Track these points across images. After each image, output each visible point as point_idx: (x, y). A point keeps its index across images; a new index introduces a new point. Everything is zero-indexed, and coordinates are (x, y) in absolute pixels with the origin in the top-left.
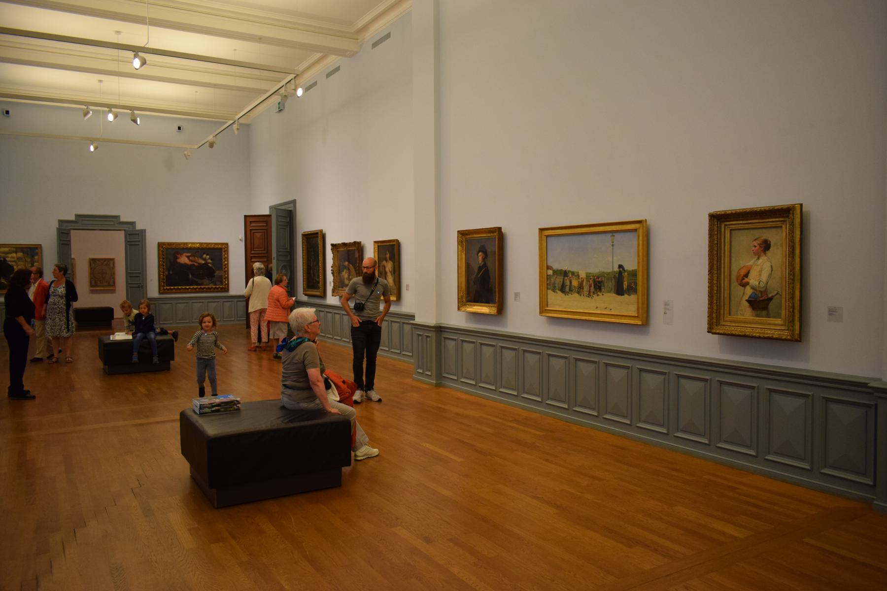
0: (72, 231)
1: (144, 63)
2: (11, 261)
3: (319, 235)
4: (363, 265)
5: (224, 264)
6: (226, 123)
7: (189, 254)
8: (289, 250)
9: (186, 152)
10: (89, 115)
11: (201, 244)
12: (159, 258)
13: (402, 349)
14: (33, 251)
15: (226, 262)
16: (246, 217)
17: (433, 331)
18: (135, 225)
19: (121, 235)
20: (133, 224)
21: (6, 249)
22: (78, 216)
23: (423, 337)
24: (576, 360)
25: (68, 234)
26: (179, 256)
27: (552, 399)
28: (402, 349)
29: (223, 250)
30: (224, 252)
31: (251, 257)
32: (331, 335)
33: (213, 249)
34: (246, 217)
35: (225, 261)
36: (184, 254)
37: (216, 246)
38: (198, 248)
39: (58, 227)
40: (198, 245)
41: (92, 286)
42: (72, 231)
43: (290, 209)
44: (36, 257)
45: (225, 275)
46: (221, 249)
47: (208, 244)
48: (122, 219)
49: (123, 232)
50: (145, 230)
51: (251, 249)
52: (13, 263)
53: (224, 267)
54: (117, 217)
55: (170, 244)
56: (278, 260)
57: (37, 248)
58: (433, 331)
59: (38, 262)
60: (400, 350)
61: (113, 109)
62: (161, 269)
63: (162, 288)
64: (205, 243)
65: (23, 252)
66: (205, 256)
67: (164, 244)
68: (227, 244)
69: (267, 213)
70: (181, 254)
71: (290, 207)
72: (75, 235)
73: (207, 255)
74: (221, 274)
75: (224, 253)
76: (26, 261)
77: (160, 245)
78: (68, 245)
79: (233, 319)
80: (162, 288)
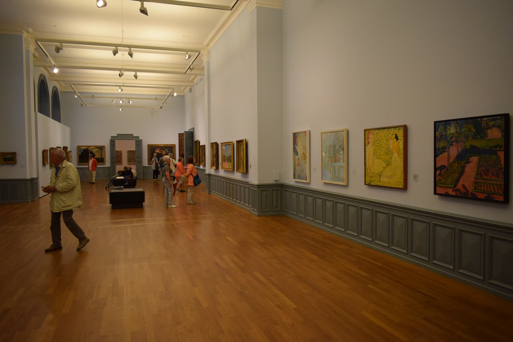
0: (116, 140)
1: (122, 90)
2: (94, 152)
4: (503, 152)
7: (159, 149)
8: (192, 147)
9: (155, 109)
10: (114, 102)
11: (165, 145)
12: (148, 152)
14: (101, 148)
16: (179, 134)
17: (256, 187)
19: (134, 141)
20: (138, 137)
21: (92, 148)
22: (118, 135)
23: (333, 203)
24: (393, 216)
25: (114, 141)
26: (156, 150)
27: (415, 252)
30: (174, 148)
31: (181, 150)
33: (169, 147)
34: (179, 134)
36: (158, 149)
37: (171, 146)
38: (163, 147)
39: (110, 139)
40: (163, 145)
41: (128, 162)
42: (116, 140)
44: (103, 151)
46: (172, 147)
47: (167, 145)
48: (134, 135)
49: (135, 140)
50: (142, 140)
52: (95, 153)
54: (132, 135)
55: (152, 145)
57: (103, 147)
58: (256, 187)
59: (103, 152)
61: (188, 52)
62: (149, 155)
63: (149, 163)
65: (98, 148)
66: (166, 149)
67: (150, 145)
68: (175, 145)
69: (183, 133)
70: (156, 149)
72: (117, 142)
73: (167, 149)
76: (99, 152)
77: (148, 145)
78: (114, 146)
80: (149, 163)
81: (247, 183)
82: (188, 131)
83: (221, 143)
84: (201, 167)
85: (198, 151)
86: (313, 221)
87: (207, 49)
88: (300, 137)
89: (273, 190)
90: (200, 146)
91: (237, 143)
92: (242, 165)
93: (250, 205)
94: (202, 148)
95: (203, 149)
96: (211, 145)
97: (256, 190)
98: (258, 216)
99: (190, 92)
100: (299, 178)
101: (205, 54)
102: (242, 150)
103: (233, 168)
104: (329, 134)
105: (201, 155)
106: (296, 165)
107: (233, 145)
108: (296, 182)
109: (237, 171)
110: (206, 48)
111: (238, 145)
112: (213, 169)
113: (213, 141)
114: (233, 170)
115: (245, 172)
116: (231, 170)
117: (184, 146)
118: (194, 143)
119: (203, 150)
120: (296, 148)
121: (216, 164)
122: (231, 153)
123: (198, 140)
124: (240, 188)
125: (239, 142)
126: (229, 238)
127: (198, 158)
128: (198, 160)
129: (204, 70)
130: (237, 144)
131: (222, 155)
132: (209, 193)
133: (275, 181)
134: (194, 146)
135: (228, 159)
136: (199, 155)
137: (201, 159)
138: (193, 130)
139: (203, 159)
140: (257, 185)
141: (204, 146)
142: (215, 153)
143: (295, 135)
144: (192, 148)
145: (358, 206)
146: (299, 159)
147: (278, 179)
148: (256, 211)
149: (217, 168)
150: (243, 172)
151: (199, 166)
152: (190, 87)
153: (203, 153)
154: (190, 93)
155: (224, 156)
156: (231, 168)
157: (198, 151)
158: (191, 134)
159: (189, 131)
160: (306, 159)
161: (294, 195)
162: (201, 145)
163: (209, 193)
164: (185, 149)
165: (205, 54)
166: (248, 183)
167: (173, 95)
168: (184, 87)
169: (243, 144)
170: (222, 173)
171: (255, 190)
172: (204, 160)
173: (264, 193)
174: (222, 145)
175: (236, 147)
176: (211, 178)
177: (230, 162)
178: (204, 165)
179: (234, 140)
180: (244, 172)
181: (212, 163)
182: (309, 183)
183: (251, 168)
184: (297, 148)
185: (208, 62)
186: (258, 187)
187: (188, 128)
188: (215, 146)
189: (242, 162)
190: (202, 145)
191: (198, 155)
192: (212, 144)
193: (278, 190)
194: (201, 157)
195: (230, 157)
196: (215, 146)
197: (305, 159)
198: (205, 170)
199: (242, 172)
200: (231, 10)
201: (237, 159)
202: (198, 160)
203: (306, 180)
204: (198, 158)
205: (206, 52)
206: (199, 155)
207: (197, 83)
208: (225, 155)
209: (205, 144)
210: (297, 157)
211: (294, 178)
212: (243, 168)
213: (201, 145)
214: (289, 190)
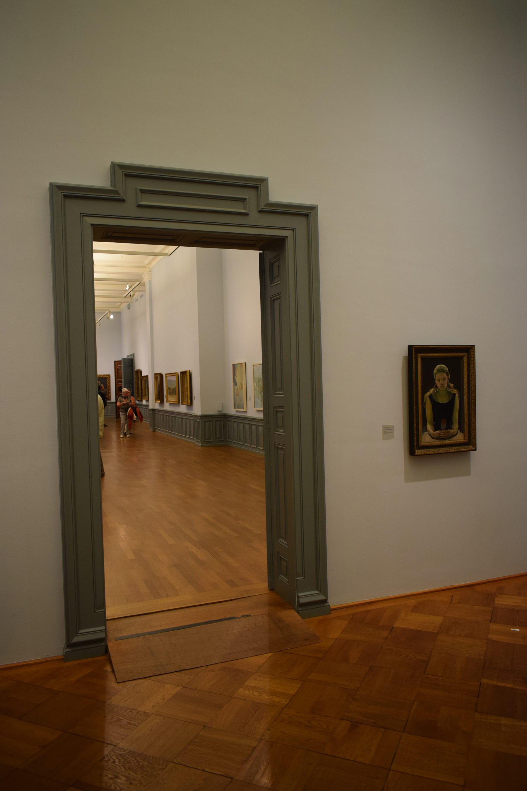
3: (139, 372)
5: (108, 385)
6: (105, 312)
13: (258, 445)
15: (109, 385)
16: (115, 361)
18: (267, 183)
28: (258, 445)
29: (107, 378)
30: (108, 379)
31: (118, 382)
32: (242, 442)
33: (102, 378)
34: (115, 361)
35: (108, 384)
37: (104, 376)
43: (132, 358)
45: (108, 391)
46: (106, 378)
51: (118, 378)
53: (108, 387)
56: (124, 383)
60: (257, 445)
64: (102, 375)
68: (109, 375)
69: (121, 360)
71: (131, 357)
74: (106, 391)
75: (107, 380)
79: (212, 440)
81: (191, 415)
82: (126, 358)
83: (166, 374)
84: (144, 402)
85: (140, 382)
86: (257, 448)
87: (149, 267)
88: (238, 369)
89: (216, 421)
90: (143, 377)
91: (182, 374)
92: (186, 397)
93: (195, 437)
94: (145, 379)
95: (146, 380)
96: (154, 376)
97: (199, 420)
98: (202, 446)
99: (129, 309)
100: (238, 407)
101: (146, 273)
102: (186, 382)
103: (178, 400)
104: (258, 366)
105: (143, 387)
106: (236, 395)
107: (177, 376)
108: (237, 411)
109: (181, 403)
110: (147, 266)
111: (182, 376)
112: (158, 403)
113: (157, 372)
114: (178, 403)
115: (189, 404)
116: (176, 403)
117: (121, 377)
118: (134, 373)
119: (146, 381)
120: (235, 379)
121: (160, 396)
122: (176, 385)
123: (140, 370)
124: (190, 422)
125: (183, 373)
126: (170, 460)
127: (140, 392)
128: (140, 394)
129: (145, 285)
130: (182, 376)
131: (167, 386)
132: (154, 431)
133: (218, 411)
134: (135, 377)
135: (173, 391)
136: (141, 387)
137: (143, 392)
138: (132, 356)
139: (146, 392)
140: (200, 416)
141: (147, 376)
142: (159, 383)
143: (234, 366)
144: (132, 380)
145: (249, 423)
146: (237, 389)
147: (221, 410)
148: (200, 442)
149: (162, 402)
150: (187, 404)
151: (142, 401)
152: (128, 304)
153: (146, 385)
154: (128, 310)
155: (169, 388)
156: (176, 401)
157: (140, 382)
158: (130, 362)
159: (128, 358)
160: (243, 389)
161: (235, 424)
162: (143, 375)
163: (154, 431)
164: (123, 381)
165: (146, 273)
166: (192, 415)
167: (108, 318)
168: (120, 303)
169: (187, 375)
170: (167, 407)
171: (198, 422)
172: (147, 393)
173: (207, 423)
174: (167, 376)
175: (181, 378)
176: (156, 414)
177: (175, 394)
178: (147, 399)
179: (179, 371)
180: (188, 404)
181: (156, 396)
182: (246, 412)
183: (195, 399)
184: (236, 378)
185: (150, 282)
186: (201, 417)
187: (125, 355)
188: (159, 377)
189: (186, 394)
190: (144, 376)
191: (140, 388)
192: (156, 375)
193: (221, 421)
194: (144, 390)
195: (175, 388)
196: (159, 377)
197: (242, 389)
198: (148, 406)
199: (186, 403)
200: (169, 256)
201: (181, 391)
202: (140, 394)
203: (244, 409)
204: (140, 392)
205: (148, 270)
206: (141, 387)
207: (137, 300)
208: (170, 387)
209: (148, 375)
210: (236, 387)
211: (235, 408)
212: (188, 400)
213: (143, 375)
214: (231, 420)
